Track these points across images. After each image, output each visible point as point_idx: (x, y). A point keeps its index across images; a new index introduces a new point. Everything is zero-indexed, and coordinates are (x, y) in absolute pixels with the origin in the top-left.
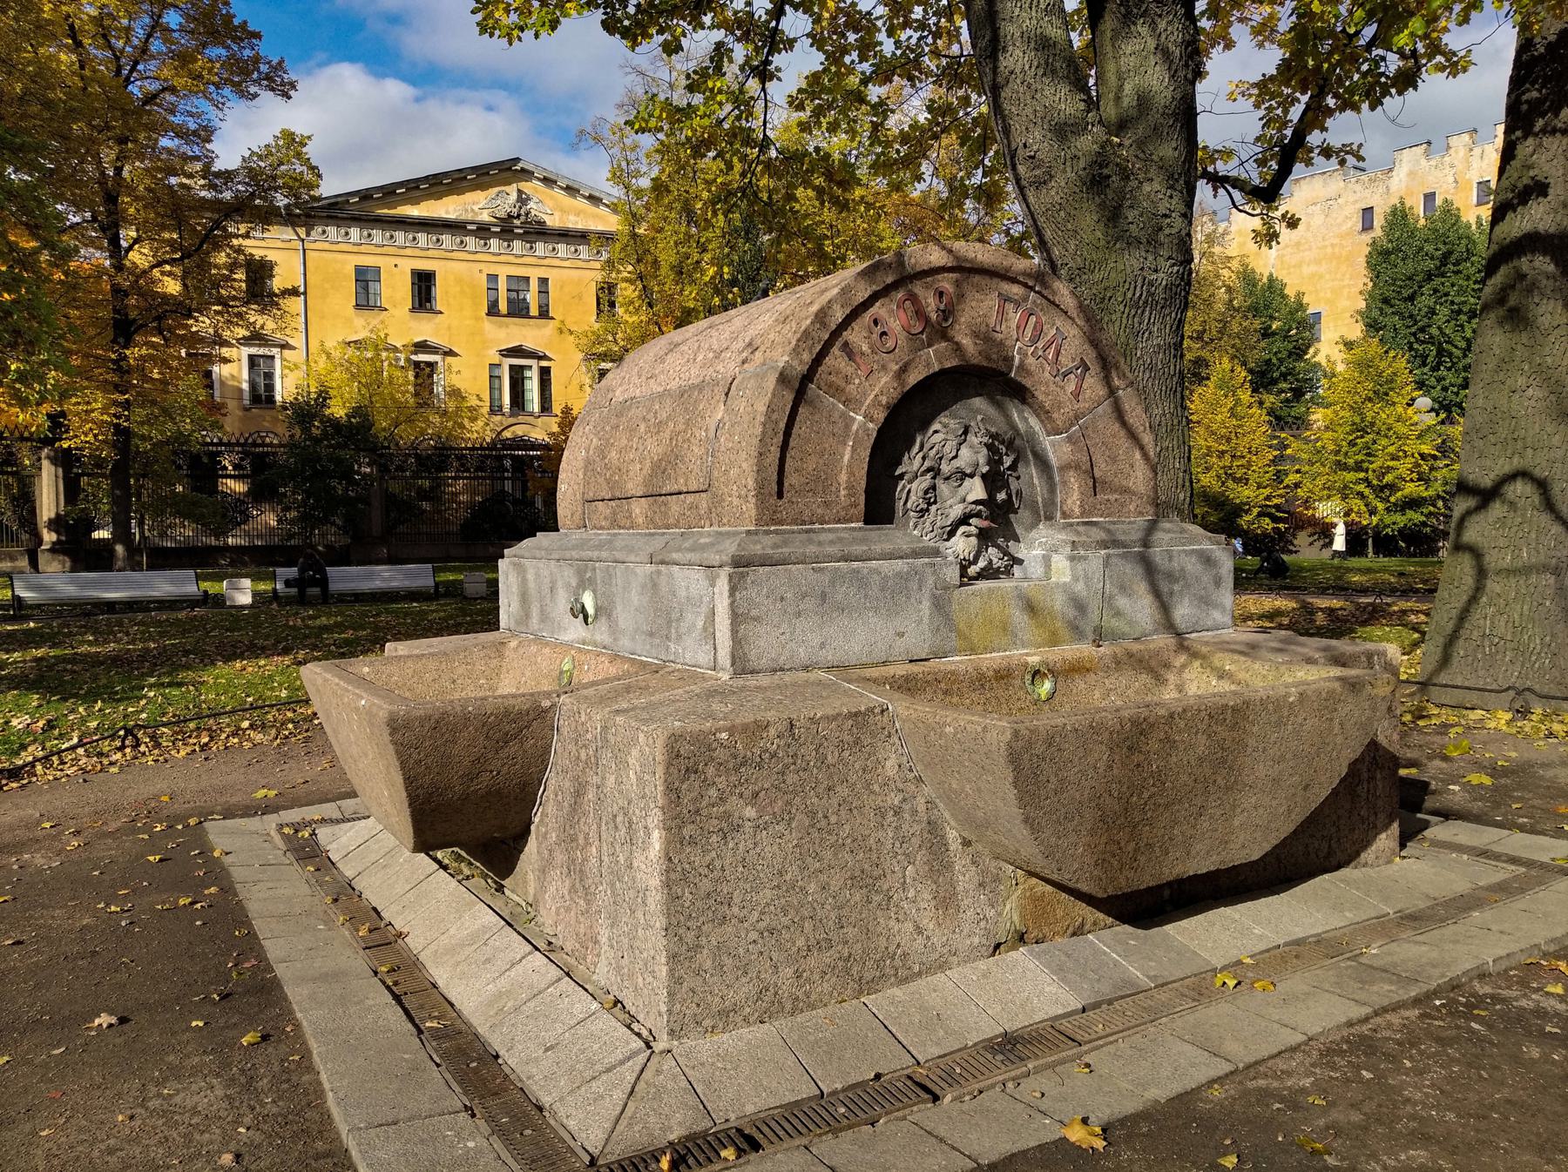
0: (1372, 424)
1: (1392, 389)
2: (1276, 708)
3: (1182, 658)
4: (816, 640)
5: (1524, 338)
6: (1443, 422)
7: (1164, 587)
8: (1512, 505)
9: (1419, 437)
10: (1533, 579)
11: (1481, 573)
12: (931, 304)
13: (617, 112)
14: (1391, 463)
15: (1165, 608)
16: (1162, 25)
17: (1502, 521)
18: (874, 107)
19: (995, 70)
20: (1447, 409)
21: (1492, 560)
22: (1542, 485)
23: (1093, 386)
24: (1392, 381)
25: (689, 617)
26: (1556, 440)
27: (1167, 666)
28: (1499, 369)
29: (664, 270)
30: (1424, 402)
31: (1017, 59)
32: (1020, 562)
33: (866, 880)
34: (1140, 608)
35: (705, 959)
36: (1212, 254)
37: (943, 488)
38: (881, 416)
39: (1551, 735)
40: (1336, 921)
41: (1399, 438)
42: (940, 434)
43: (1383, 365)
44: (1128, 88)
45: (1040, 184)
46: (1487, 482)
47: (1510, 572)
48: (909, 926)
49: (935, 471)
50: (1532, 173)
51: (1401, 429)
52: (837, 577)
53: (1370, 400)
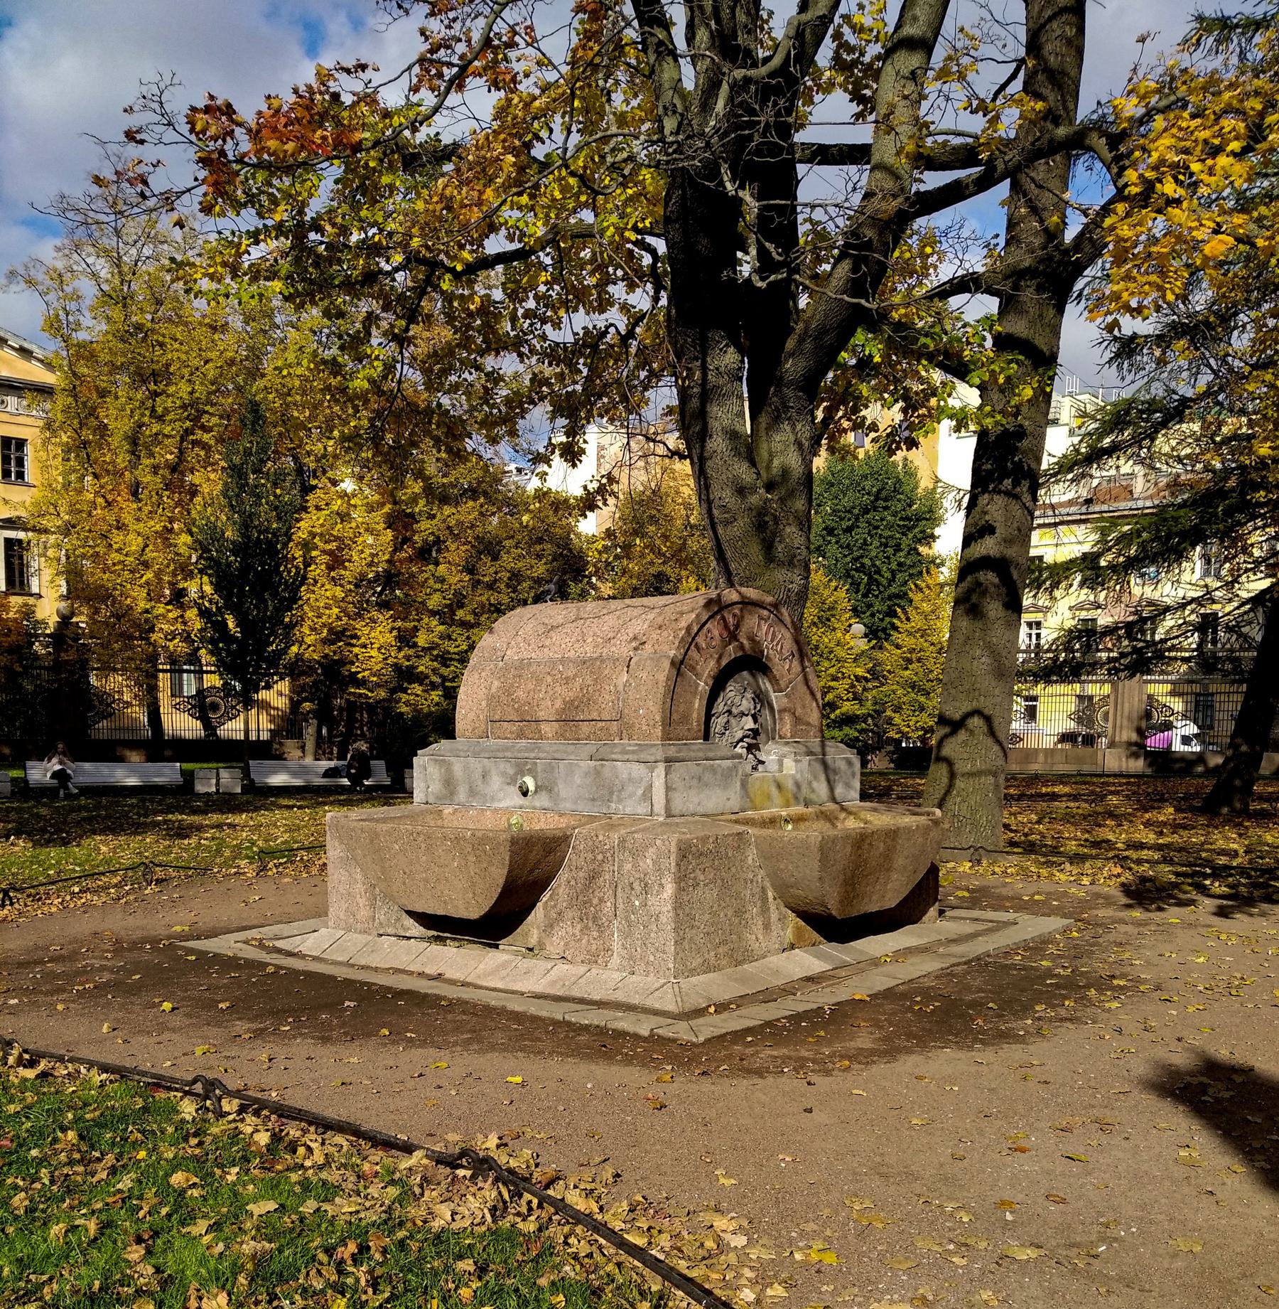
0: (817, 647)
1: (833, 616)
2: (908, 830)
3: (843, 815)
4: (696, 800)
5: (979, 624)
6: (873, 648)
7: (832, 777)
8: (972, 732)
9: (855, 660)
10: (983, 779)
11: (952, 776)
12: (731, 620)
13: (55, 254)
14: (832, 684)
15: (832, 789)
16: (799, 427)
17: (965, 743)
18: (487, 375)
19: (703, 447)
20: (877, 634)
21: (960, 767)
22: (988, 720)
23: (796, 663)
24: (833, 608)
25: (630, 789)
26: (997, 692)
27: (836, 818)
28: (965, 643)
29: (115, 441)
30: (859, 628)
31: (717, 443)
32: (763, 763)
33: (739, 913)
34: (822, 788)
35: (686, 943)
36: (673, 471)
37: (733, 721)
38: (711, 682)
39: (994, 873)
40: (925, 941)
41: (838, 661)
42: (732, 689)
43: (826, 593)
44: (776, 463)
45: (727, 523)
46: (957, 716)
47: (970, 775)
48: (754, 937)
49: (729, 712)
50: (987, 518)
51: (840, 652)
52: (705, 769)
53: (814, 624)
